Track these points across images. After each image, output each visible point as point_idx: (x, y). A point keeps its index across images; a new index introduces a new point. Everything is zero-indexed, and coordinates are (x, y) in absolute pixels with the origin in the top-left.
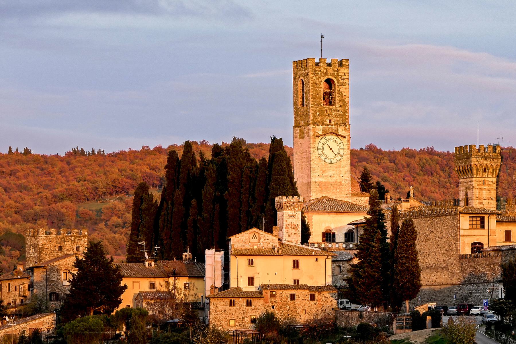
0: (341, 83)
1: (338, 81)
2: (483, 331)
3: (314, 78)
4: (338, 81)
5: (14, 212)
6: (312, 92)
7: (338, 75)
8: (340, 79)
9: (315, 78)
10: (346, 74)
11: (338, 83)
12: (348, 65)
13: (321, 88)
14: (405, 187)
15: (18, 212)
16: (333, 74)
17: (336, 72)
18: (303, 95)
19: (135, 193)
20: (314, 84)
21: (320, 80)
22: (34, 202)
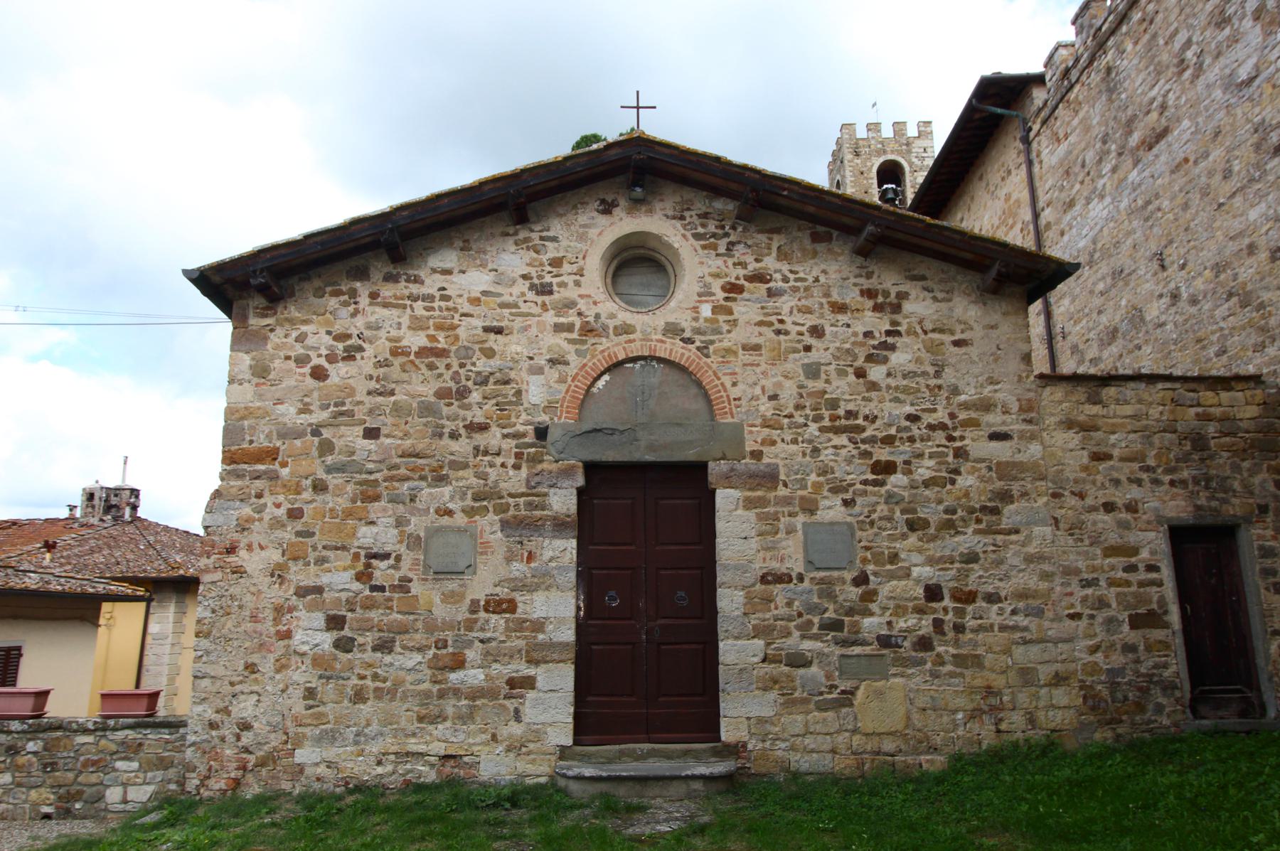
0: (917, 166)
1: (911, 164)
2: (178, 622)
3: (856, 161)
4: (911, 164)
5: (250, 661)
6: (852, 187)
7: (909, 152)
8: (914, 160)
9: (859, 161)
10: (928, 150)
11: (911, 167)
12: (931, 132)
13: (872, 178)
14: (408, 500)
15: (247, 843)
16: (897, 151)
17: (904, 147)
18: (1049, 117)
19: (251, 367)
20: (857, 173)
21: (869, 164)
22: (1252, 171)
